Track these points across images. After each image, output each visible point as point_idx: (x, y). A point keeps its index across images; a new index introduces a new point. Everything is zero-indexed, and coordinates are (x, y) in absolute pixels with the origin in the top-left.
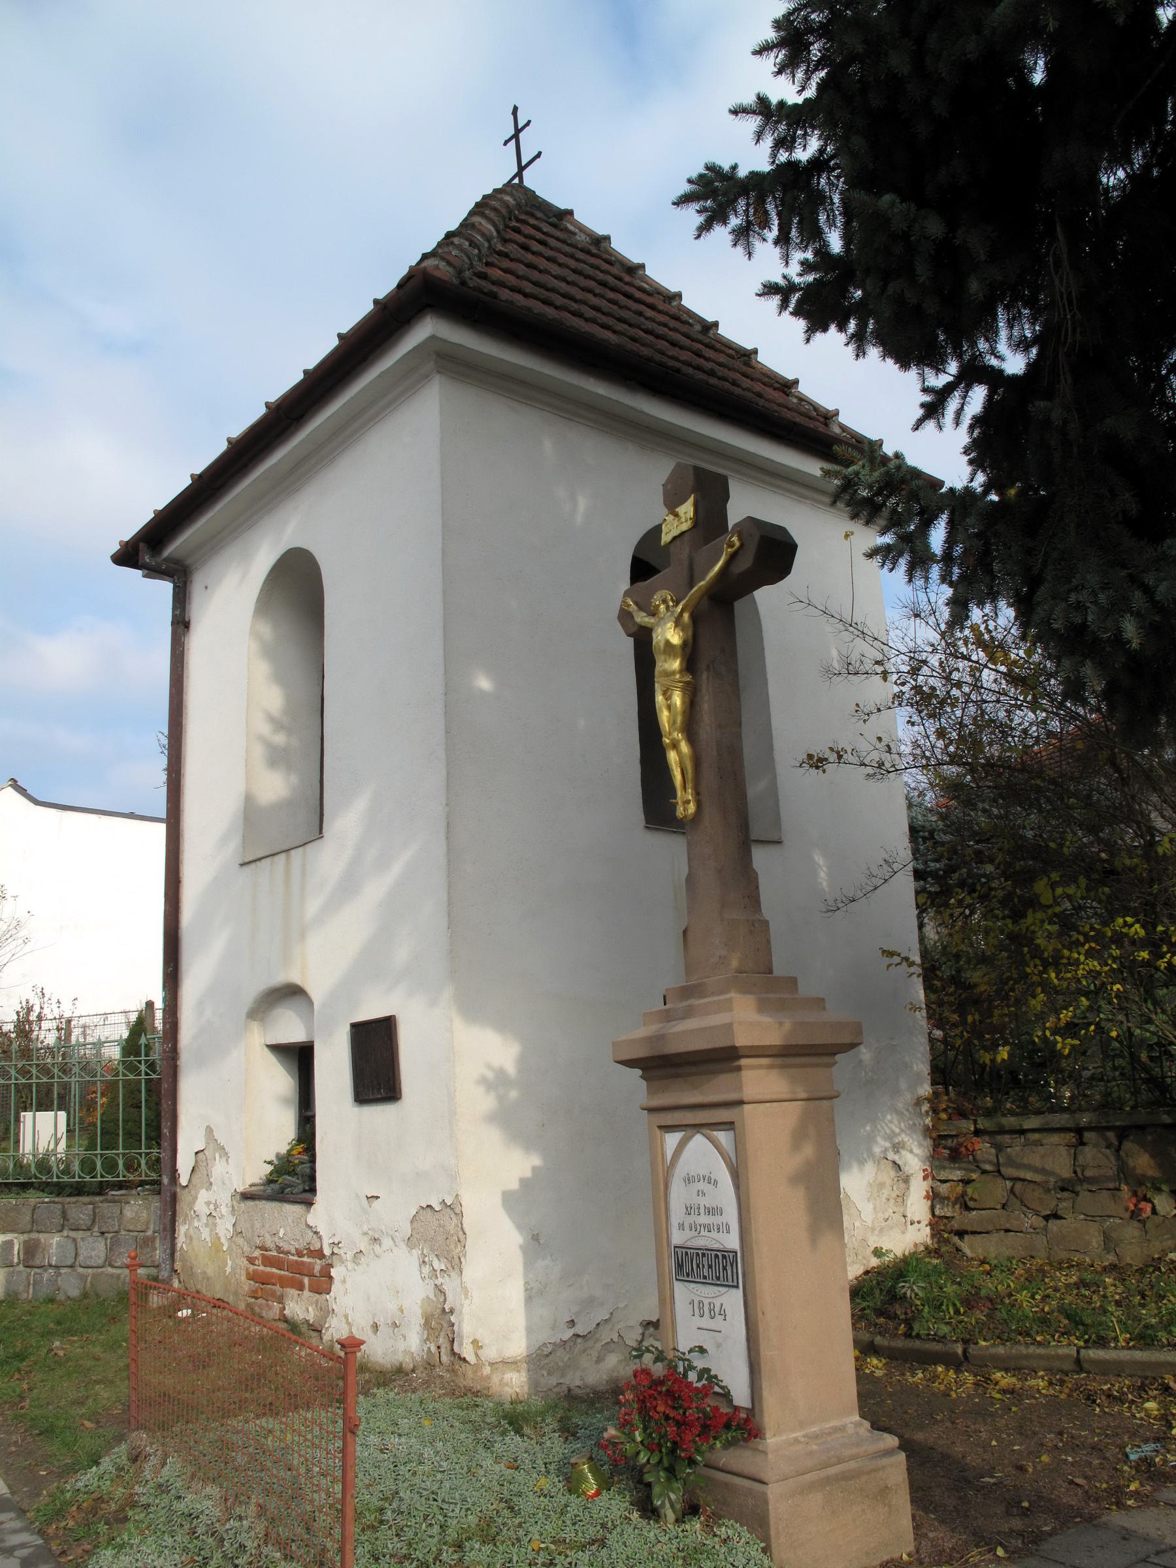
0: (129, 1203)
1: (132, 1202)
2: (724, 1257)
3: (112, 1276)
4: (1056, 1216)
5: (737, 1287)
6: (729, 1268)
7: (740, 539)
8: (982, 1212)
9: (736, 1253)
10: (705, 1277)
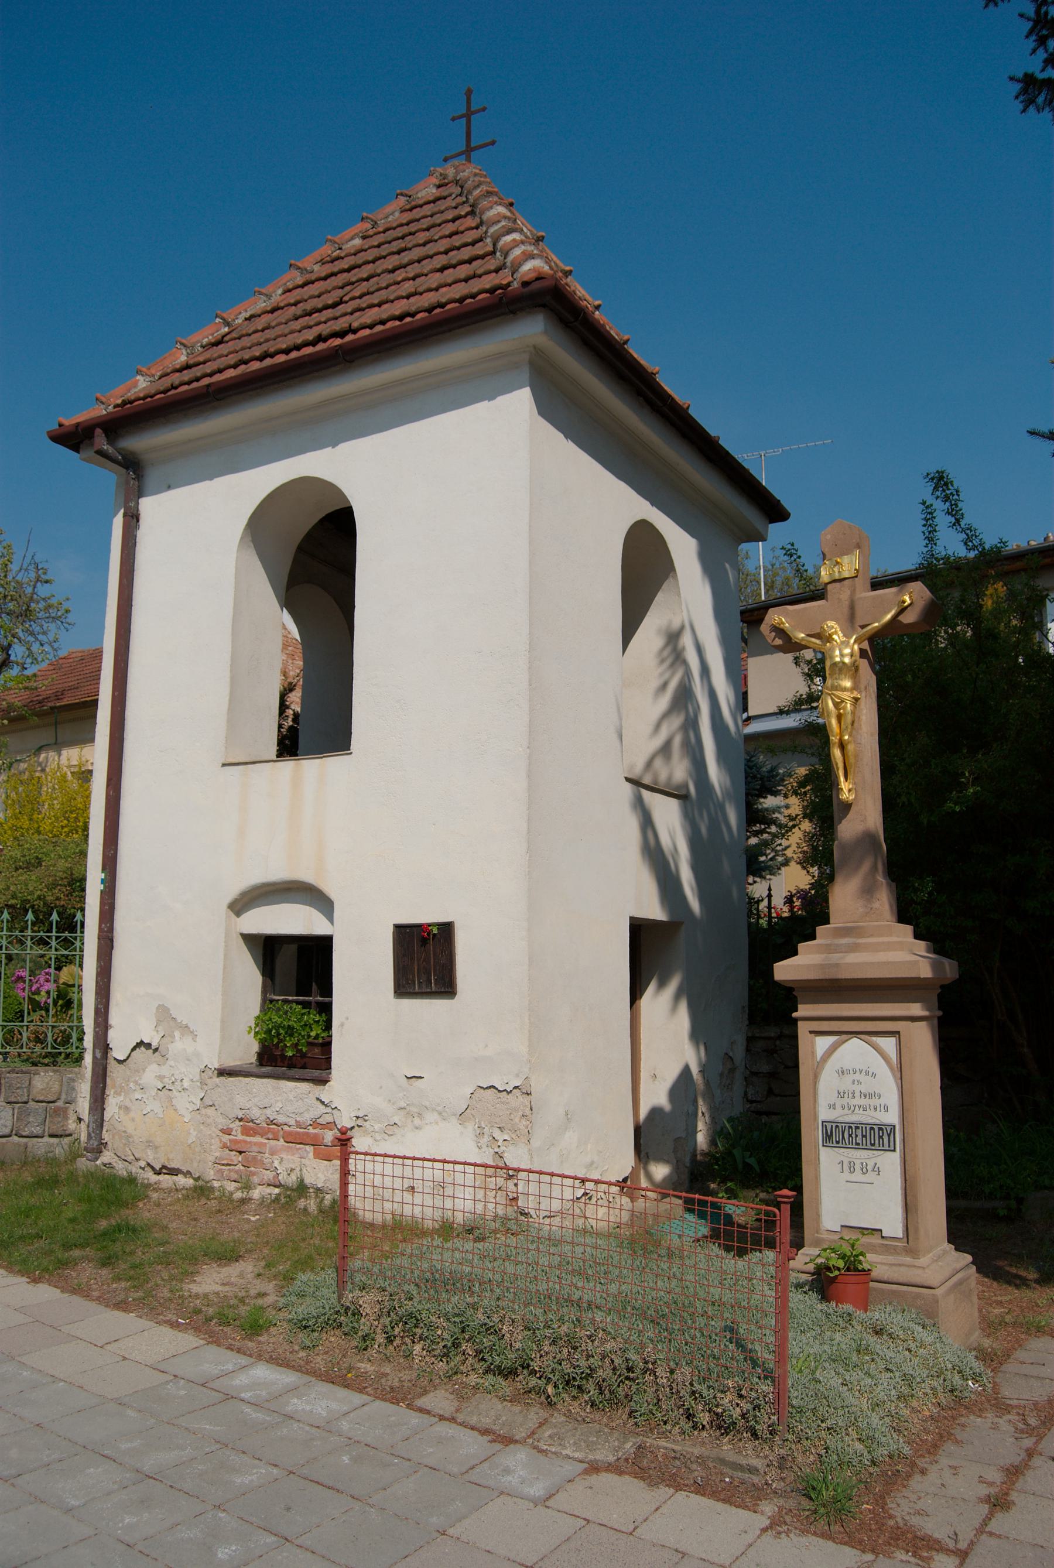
0: (38, 1074)
1: (42, 1074)
2: (880, 1129)
3: (19, 1144)
5: (894, 1150)
7: (910, 597)
9: (894, 1126)
10: (857, 1144)
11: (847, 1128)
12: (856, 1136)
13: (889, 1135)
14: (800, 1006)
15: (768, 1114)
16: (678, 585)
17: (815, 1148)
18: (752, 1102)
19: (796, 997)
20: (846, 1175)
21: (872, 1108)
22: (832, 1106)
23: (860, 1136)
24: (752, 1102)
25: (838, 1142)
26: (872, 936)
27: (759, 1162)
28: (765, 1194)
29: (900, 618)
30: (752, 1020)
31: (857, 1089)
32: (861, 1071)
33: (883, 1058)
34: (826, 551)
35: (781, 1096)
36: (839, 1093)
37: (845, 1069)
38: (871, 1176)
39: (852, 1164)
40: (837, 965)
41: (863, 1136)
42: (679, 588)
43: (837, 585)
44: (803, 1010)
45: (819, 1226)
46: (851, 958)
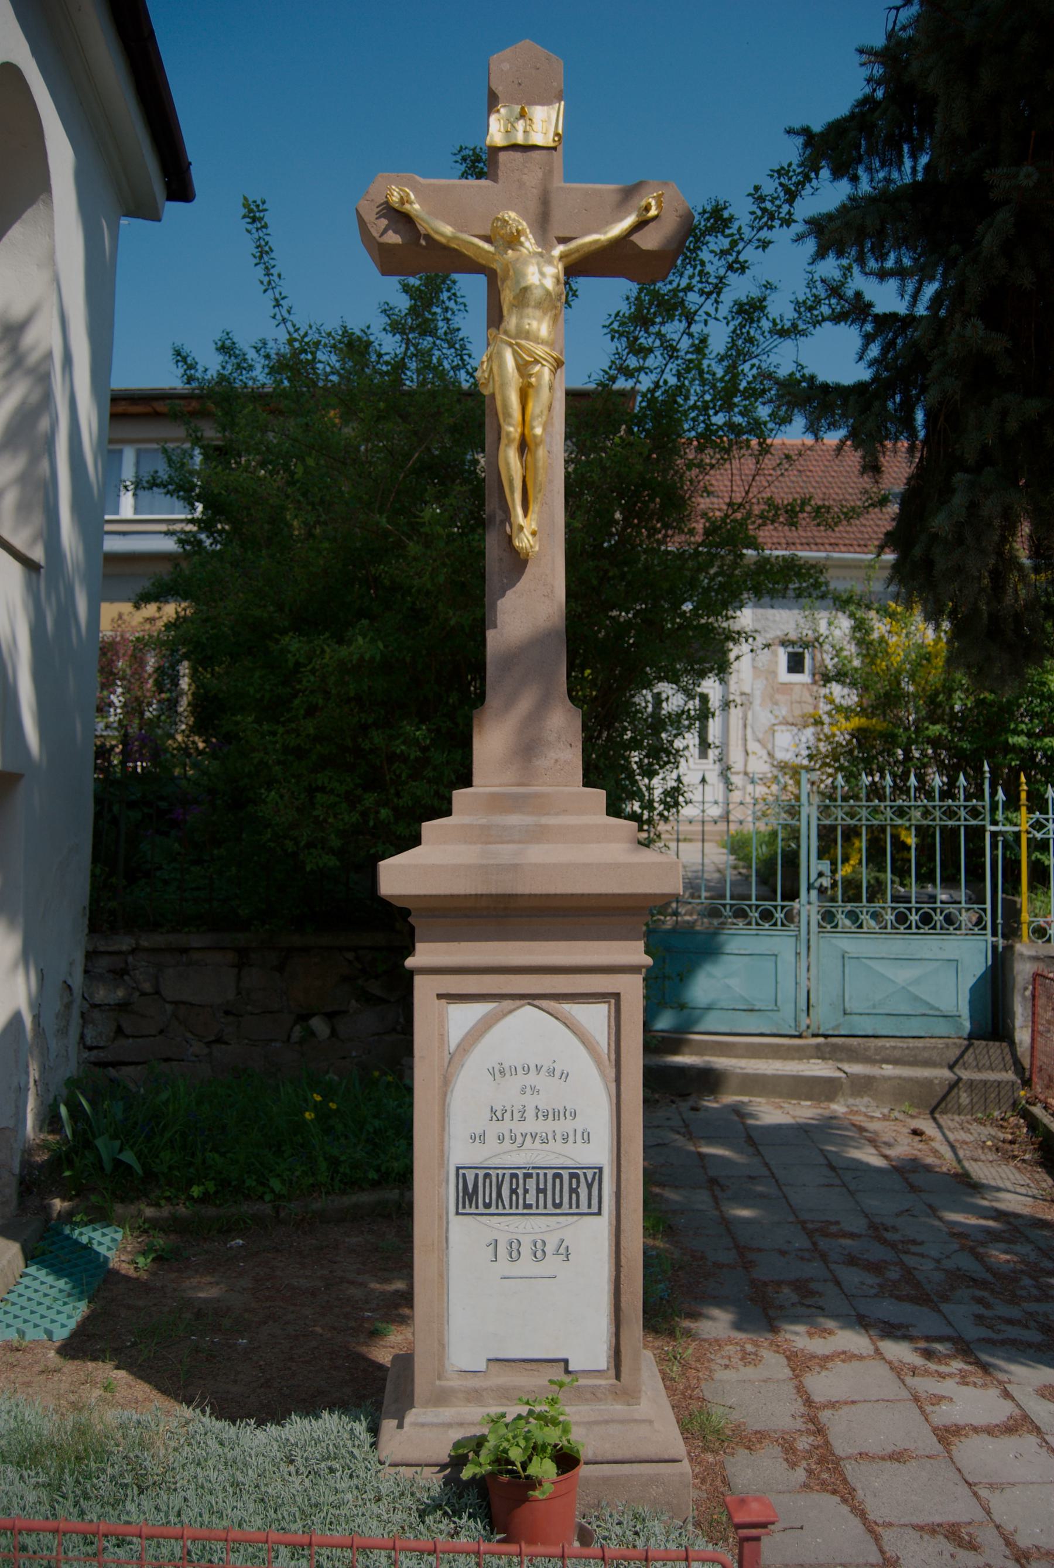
2: (572, 1176)
4: (218, 1040)
5: (599, 1213)
6: (583, 1191)
8: (139, 1040)
9: (601, 1169)
10: (530, 1206)
11: (507, 1178)
12: (526, 1191)
13: (590, 1186)
14: (419, 946)
15: (114, 1064)
16: (52, 217)
17: (440, 1217)
18: (90, 1049)
19: (412, 929)
20: (504, 1266)
21: (558, 1137)
22: (480, 1138)
23: (533, 1191)
24: (90, 1049)
25: (487, 1206)
26: (565, 812)
27: (139, 1158)
28: (152, 1209)
29: (636, 238)
30: (94, 928)
31: (531, 1102)
32: (538, 1069)
33: (583, 1043)
34: (499, 89)
35: (133, 1037)
36: (493, 1111)
37: (506, 1066)
38: (552, 1264)
39: (515, 1245)
40: (515, 867)
41: (539, 1191)
42: (53, 223)
43: (518, 155)
44: (423, 955)
45: (443, 1366)
46: (537, 854)
